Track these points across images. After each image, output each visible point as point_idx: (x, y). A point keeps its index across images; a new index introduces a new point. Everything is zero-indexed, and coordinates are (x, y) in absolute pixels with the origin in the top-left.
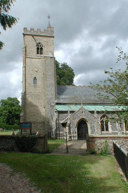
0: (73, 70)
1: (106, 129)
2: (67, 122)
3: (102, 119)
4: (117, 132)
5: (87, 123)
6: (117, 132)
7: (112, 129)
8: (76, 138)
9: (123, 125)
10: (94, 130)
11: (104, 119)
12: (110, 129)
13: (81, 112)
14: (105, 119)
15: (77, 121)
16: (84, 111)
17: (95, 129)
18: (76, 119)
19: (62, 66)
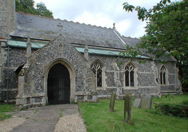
0: (52, 13)
1: (129, 83)
2: (23, 66)
3: (93, 67)
4: (115, 87)
5: (69, 70)
6: (115, 87)
7: (108, 83)
8: (44, 101)
9: (123, 78)
10: (82, 83)
11: (95, 67)
12: (136, 82)
13: (58, 44)
14: (98, 67)
15: (48, 63)
16: (65, 45)
17: (85, 82)
18: (44, 59)
19: (38, 6)
